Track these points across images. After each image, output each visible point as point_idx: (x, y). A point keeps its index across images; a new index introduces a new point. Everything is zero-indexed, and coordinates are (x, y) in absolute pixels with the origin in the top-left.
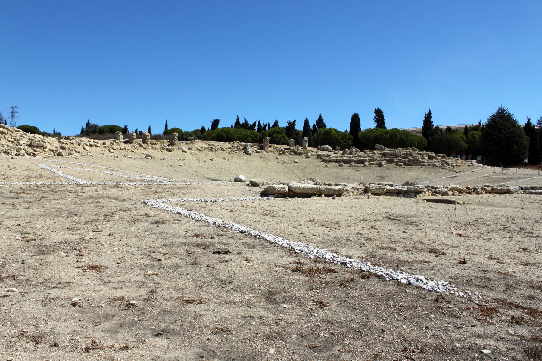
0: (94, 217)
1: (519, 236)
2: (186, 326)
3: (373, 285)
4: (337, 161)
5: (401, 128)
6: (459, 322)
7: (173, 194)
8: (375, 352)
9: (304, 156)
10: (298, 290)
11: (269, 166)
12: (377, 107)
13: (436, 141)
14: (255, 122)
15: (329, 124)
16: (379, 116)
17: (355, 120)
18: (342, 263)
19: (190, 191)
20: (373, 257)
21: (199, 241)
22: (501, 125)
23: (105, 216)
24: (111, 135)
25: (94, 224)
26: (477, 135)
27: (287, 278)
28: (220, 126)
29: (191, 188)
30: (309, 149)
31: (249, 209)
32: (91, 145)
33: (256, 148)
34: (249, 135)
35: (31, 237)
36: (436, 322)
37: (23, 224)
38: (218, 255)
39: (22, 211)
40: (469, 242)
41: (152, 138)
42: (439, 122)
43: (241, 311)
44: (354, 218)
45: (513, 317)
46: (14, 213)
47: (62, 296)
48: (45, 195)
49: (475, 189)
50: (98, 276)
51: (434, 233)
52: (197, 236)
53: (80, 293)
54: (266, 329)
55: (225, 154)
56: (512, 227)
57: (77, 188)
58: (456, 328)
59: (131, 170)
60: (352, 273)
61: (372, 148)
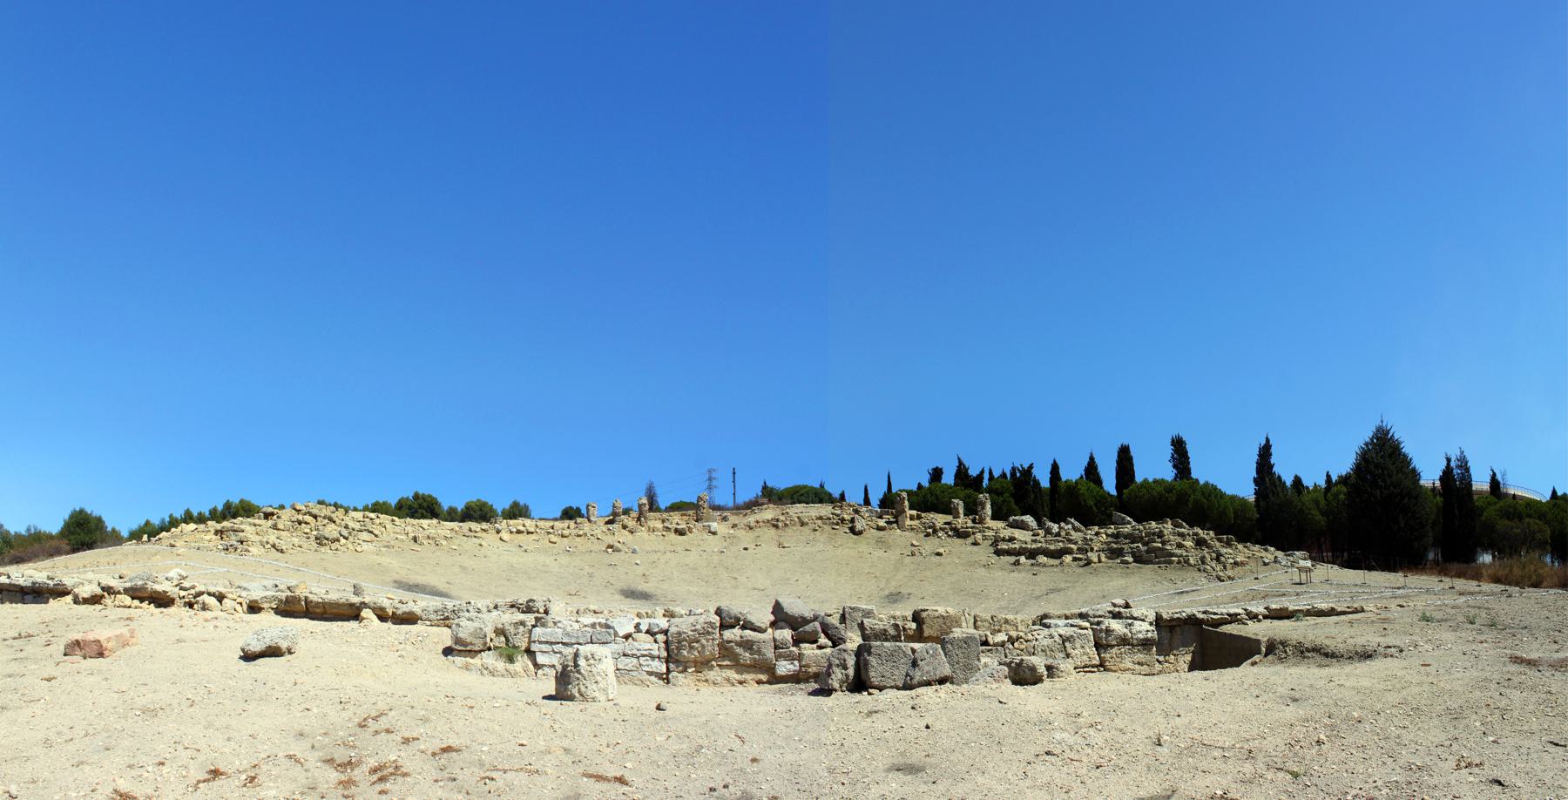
9: (970, 540)
12: (1175, 433)
13: (1279, 518)
22: (1377, 466)
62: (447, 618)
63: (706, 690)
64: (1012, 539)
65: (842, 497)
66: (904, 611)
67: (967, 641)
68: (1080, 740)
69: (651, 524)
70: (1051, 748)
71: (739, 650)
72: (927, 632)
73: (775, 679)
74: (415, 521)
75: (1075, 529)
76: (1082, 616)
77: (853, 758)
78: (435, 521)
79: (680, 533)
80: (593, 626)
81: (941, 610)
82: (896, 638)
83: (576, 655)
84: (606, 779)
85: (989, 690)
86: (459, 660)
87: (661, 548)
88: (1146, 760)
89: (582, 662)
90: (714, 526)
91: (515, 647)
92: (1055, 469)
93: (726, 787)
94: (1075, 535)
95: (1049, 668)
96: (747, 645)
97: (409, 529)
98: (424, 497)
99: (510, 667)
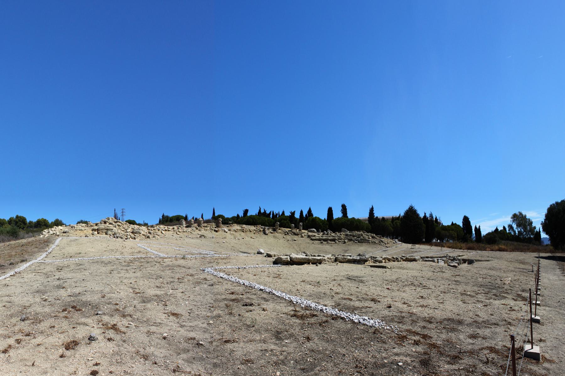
0: (172, 280)
1: (420, 289)
2: (224, 360)
3: (339, 324)
4: (319, 240)
5: (356, 217)
6: (386, 346)
7: (218, 263)
8: (339, 370)
9: (300, 236)
10: (294, 330)
11: (278, 243)
12: (343, 203)
13: (377, 227)
15: (315, 214)
16: (344, 209)
17: (330, 211)
18: (321, 310)
19: (229, 261)
20: (339, 305)
21: (233, 297)
23: (179, 279)
24: (177, 222)
25: (172, 284)
26: (398, 223)
27: (288, 321)
28: (249, 214)
29: (230, 258)
30: (303, 231)
31: (266, 274)
32: (166, 230)
33: (271, 230)
34: (267, 221)
35: (137, 291)
36: (374, 346)
37: (133, 283)
38: (245, 307)
39: (131, 274)
40: (393, 293)
41: (204, 223)
42: (378, 214)
43: (260, 346)
44: (328, 279)
45: (415, 341)
46: (128, 275)
47: (157, 331)
48: (142, 264)
49: (397, 258)
50: (177, 320)
51: (374, 288)
52: (233, 293)
53: (167, 331)
54: (275, 358)
55: (252, 235)
56: (416, 283)
57: (160, 260)
58: (385, 350)
59: (191, 246)
60: (327, 317)
61: (340, 231)
98: (20, 217)
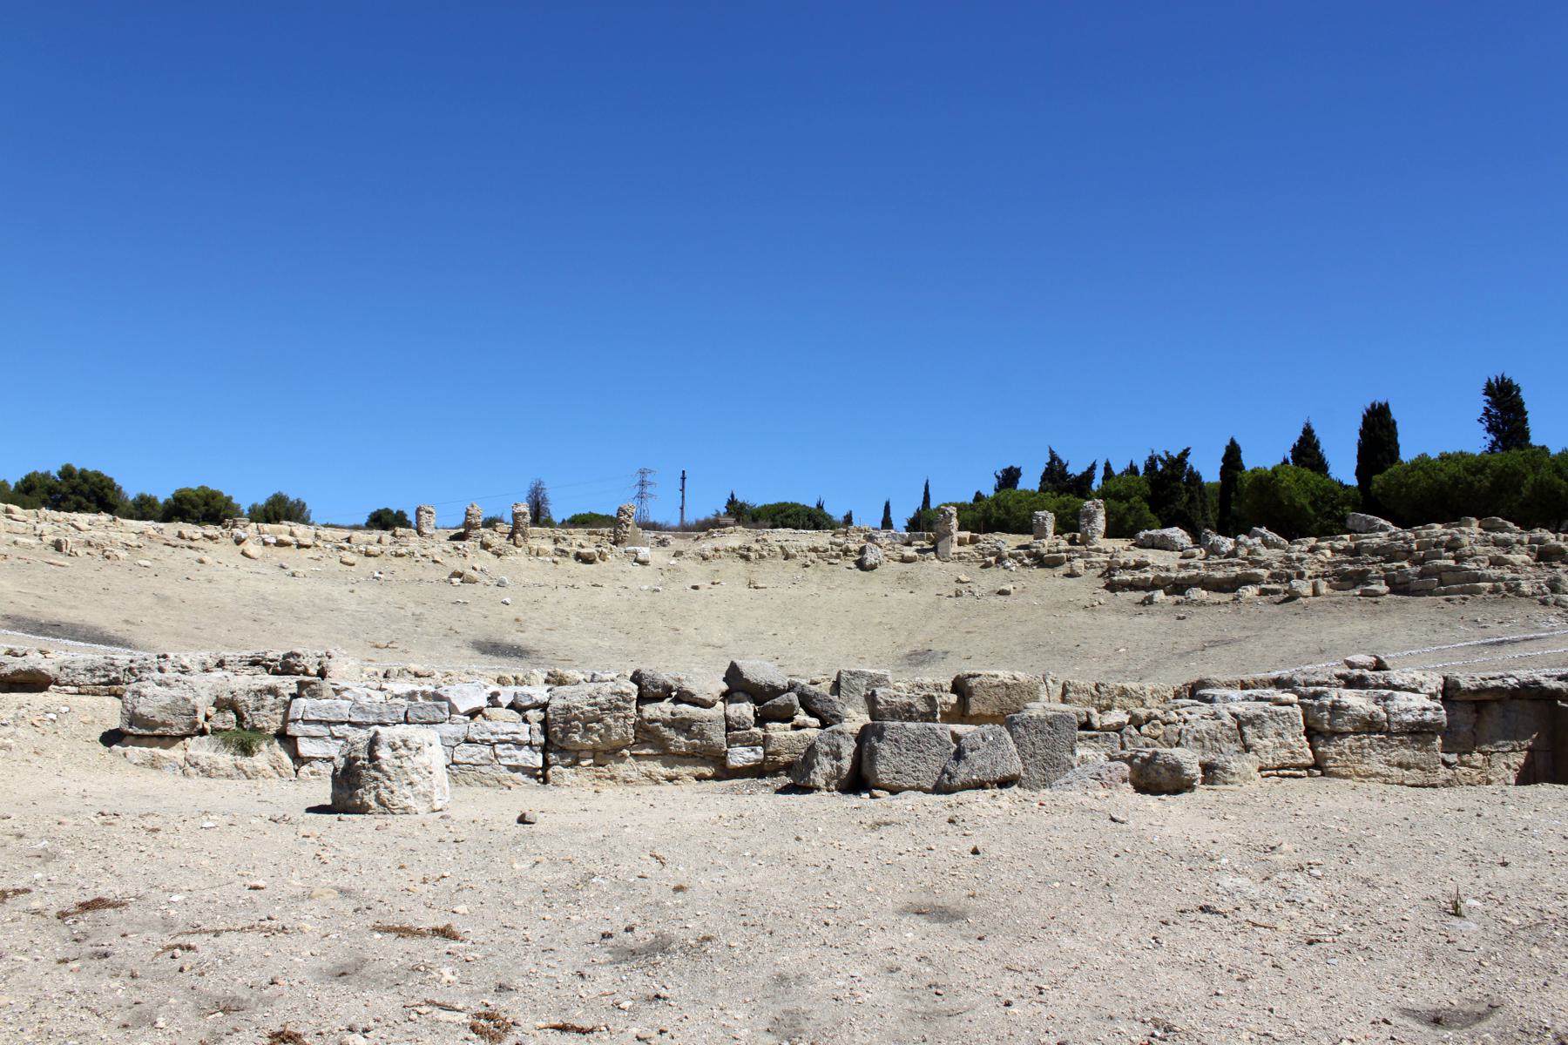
12: (1493, 374)
14: (1093, 467)
62: (116, 681)
63: (609, 791)
64: (1140, 566)
65: (848, 520)
66: (939, 677)
67: (1053, 722)
68: (1273, 892)
69: (535, 544)
70: (1212, 901)
71: (668, 733)
72: (975, 707)
73: (725, 772)
74: (62, 515)
75: (1267, 544)
76: (1279, 683)
77: (845, 888)
78: (104, 517)
79: (586, 560)
80: (412, 696)
81: (1004, 675)
82: (928, 717)
83: (374, 742)
84: (419, 933)
85: (1090, 805)
86: (136, 752)
87: (551, 581)
88: (1423, 940)
89: (384, 753)
90: (644, 552)
91: (254, 729)
92: (1232, 455)
93: (629, 929)
94: (1265, 554)
95: (1208, 769)
96: (683, 726)
97: (45, 527)
98: (84, 475)
99: (245, 762)
